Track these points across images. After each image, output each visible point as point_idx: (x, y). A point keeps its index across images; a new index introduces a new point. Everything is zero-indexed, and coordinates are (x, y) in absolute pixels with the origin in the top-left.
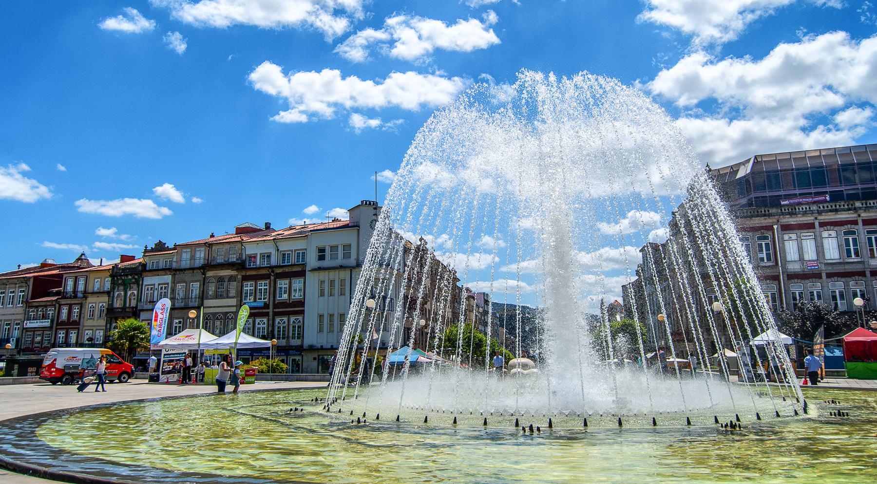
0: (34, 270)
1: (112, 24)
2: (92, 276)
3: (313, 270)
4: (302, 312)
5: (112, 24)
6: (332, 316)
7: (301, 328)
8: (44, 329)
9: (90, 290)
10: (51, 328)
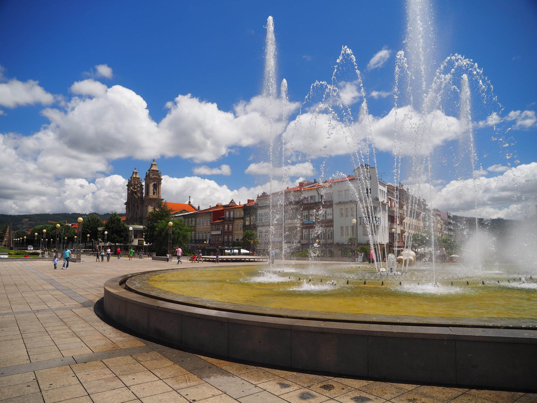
0: (214, 208)
1: (270, 18)
2: (236, 210)
3: (337, 204)
4: (332, 226)
5: (270, 18)
6: (347, 227)
7: (332, 233)
8: (218, 235)
9: (236, 217)
10: (221, 234)
